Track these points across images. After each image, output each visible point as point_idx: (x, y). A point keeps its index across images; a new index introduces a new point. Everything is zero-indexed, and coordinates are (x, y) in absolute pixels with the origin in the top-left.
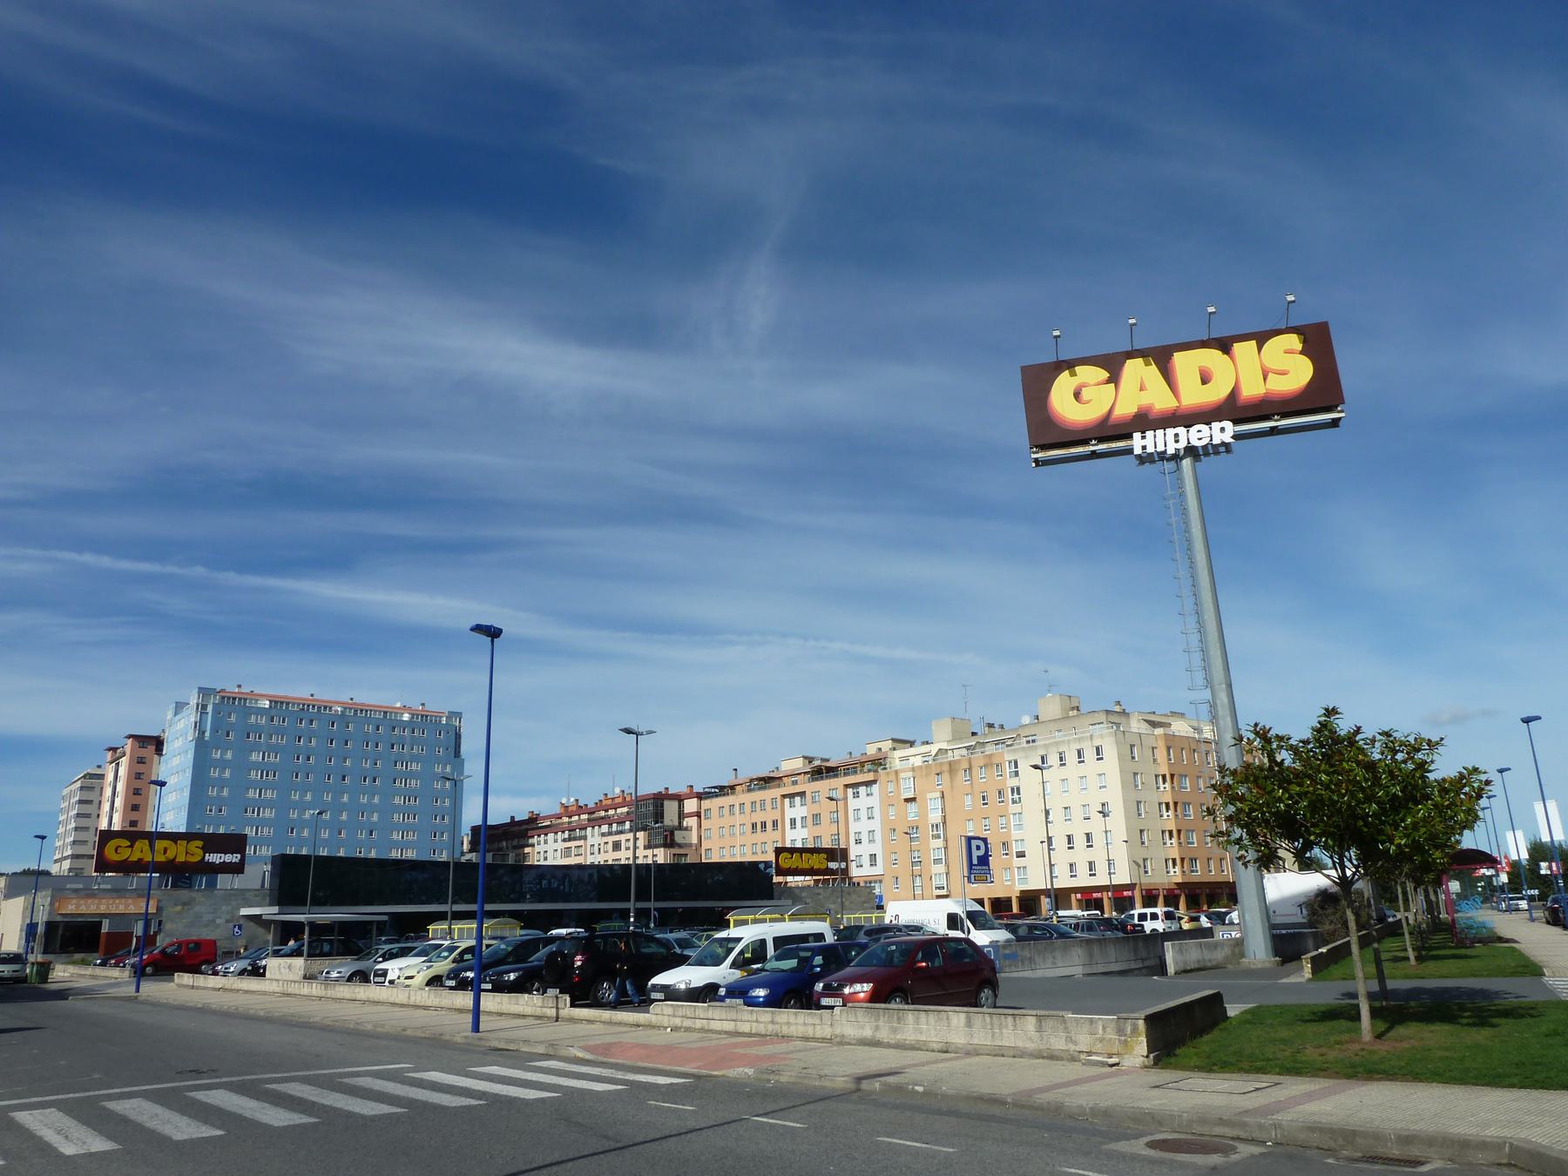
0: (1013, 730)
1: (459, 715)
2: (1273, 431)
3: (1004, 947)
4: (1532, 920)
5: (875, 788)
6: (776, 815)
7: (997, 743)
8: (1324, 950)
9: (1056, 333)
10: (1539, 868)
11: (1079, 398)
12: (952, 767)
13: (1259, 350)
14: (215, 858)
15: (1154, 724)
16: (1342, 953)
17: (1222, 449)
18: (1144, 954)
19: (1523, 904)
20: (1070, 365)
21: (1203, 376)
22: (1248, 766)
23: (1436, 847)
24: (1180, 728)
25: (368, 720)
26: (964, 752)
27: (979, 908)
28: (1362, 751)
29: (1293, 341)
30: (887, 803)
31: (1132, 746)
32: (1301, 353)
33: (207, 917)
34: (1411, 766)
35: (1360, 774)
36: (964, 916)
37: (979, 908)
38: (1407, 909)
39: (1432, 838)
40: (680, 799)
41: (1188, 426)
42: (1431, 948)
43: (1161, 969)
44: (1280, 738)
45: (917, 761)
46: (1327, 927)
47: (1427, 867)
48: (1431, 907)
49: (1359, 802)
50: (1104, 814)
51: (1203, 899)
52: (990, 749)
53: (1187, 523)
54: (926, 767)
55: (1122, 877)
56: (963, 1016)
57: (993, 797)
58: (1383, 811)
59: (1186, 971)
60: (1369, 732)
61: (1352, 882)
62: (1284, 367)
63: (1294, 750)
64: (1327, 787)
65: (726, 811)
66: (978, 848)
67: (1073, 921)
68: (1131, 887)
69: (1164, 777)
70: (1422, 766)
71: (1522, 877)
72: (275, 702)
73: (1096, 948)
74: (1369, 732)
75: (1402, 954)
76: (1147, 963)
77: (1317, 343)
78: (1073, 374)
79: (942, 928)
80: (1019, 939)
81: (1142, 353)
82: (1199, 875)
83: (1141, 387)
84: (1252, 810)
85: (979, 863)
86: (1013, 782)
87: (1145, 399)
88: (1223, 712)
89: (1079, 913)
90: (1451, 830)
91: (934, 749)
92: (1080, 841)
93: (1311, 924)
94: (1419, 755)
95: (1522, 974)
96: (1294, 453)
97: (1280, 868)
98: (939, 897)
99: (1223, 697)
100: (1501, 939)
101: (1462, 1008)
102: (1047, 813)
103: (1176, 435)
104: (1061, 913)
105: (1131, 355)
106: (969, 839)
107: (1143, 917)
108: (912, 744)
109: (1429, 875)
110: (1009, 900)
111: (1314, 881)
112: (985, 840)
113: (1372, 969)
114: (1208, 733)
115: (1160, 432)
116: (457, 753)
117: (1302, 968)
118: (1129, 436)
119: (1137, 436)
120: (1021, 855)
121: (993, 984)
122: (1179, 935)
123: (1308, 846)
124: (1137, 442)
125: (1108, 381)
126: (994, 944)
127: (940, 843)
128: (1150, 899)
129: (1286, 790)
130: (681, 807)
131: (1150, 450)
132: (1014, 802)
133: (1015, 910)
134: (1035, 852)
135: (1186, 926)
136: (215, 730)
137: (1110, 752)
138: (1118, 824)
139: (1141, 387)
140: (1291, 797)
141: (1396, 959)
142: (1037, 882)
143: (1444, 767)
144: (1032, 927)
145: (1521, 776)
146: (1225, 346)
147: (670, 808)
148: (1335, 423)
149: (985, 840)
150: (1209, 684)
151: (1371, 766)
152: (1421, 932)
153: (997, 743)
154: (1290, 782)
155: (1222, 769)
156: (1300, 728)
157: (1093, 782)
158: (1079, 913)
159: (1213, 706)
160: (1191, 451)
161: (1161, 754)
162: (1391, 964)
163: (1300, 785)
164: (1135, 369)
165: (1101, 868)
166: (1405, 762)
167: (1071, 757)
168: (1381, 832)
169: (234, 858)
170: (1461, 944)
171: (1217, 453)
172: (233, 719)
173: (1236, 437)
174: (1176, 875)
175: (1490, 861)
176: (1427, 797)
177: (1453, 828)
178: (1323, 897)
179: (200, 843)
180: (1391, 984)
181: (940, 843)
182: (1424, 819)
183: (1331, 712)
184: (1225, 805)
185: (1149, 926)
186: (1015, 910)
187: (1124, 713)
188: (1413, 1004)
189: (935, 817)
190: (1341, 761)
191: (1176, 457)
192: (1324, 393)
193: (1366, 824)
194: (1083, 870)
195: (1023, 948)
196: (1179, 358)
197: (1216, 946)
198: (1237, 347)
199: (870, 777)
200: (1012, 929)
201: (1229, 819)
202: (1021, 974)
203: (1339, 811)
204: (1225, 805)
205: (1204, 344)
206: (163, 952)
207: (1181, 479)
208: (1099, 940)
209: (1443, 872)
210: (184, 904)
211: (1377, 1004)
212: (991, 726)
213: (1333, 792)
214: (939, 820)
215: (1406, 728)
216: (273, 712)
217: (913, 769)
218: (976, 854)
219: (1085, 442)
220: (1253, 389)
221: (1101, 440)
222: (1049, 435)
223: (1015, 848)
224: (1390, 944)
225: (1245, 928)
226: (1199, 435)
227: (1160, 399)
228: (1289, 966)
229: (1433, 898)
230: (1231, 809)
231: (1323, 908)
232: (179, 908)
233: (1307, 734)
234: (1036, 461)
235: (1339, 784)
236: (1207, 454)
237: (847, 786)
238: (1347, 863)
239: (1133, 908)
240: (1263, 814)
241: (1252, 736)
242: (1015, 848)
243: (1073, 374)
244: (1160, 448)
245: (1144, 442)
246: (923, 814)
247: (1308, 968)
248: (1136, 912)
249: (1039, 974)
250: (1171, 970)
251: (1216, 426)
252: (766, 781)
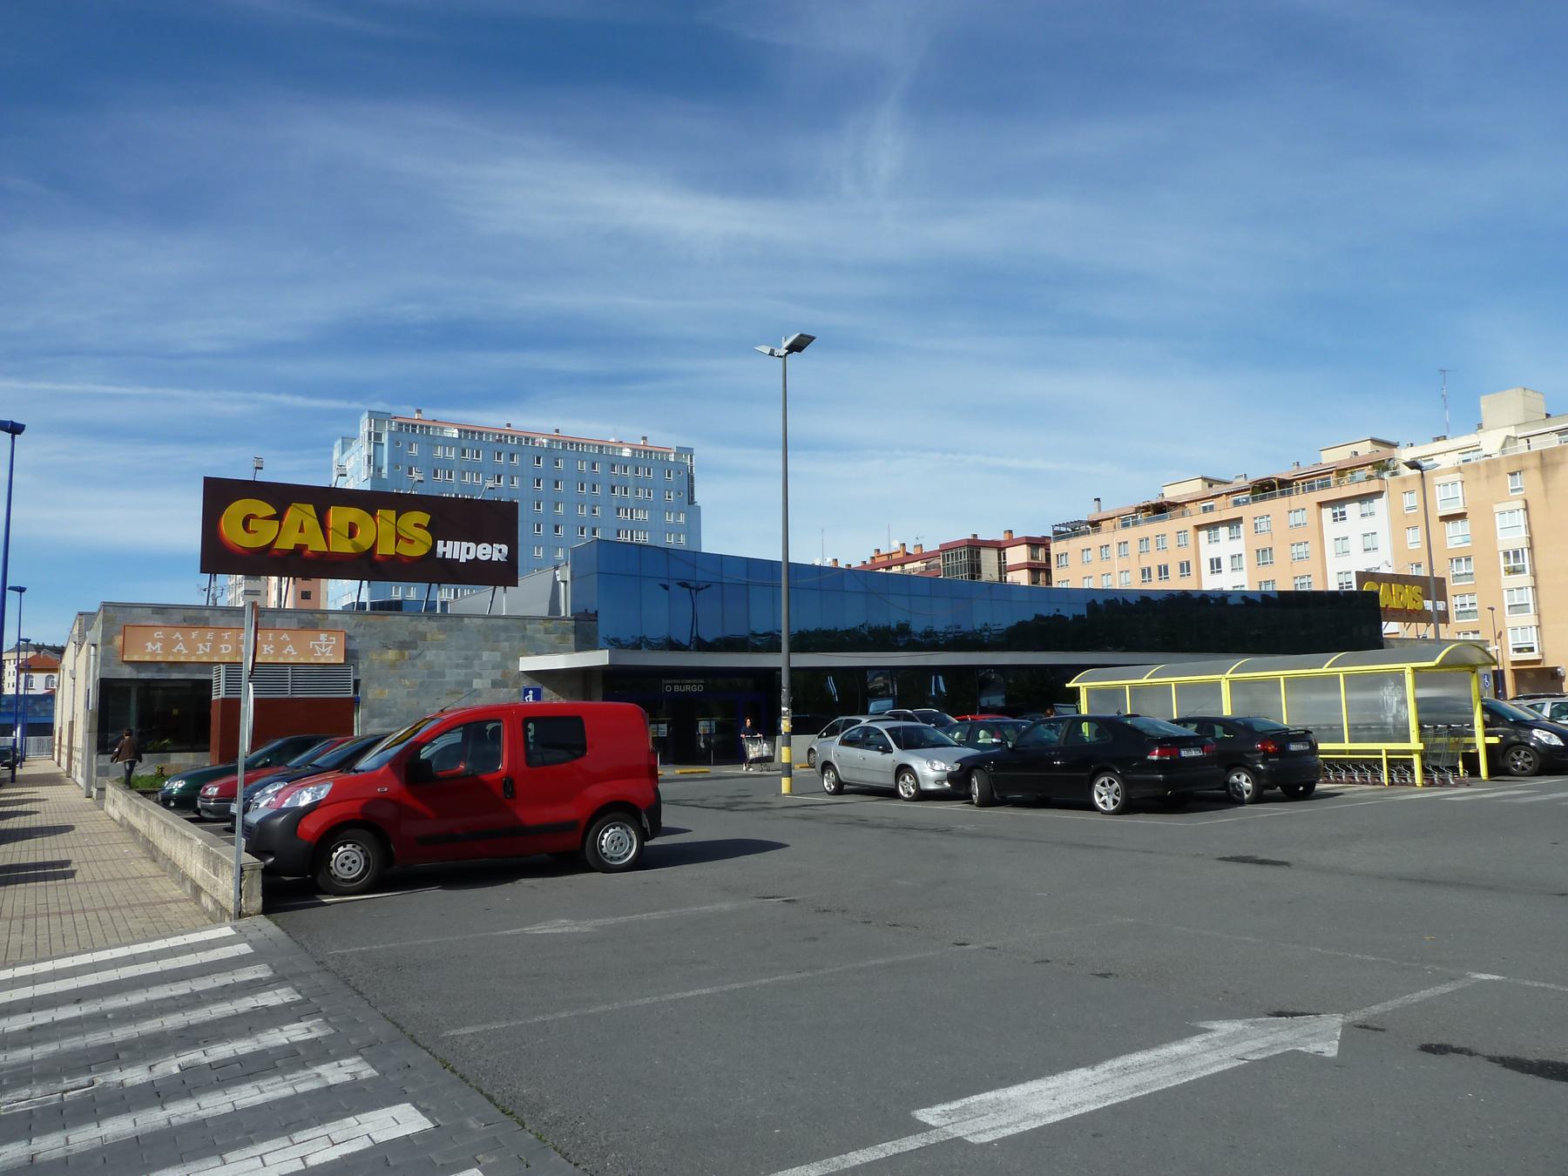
1: (690, 451)
5: (1379, 505)
6: (1186, 555)
14: (457, 550)
25: (581, 456)
30: (1400, 523)
33: (453, 676)
40: (1000, 547)
65: (1114, 549)
72: (465, 432)
116: (691, 501)
130: (1001, 557)
136: (394, 465)
147: (989, 559)
169: (493, 552)
172: (415, 451)
179: (424, 518)
199: (1374, 486)
206: (409, 765)
210: (402, 646)
214: (1524, 544)
216: (464, 443)
232: (392, 655)
237: (1321, 505)
252: (1160, 510)
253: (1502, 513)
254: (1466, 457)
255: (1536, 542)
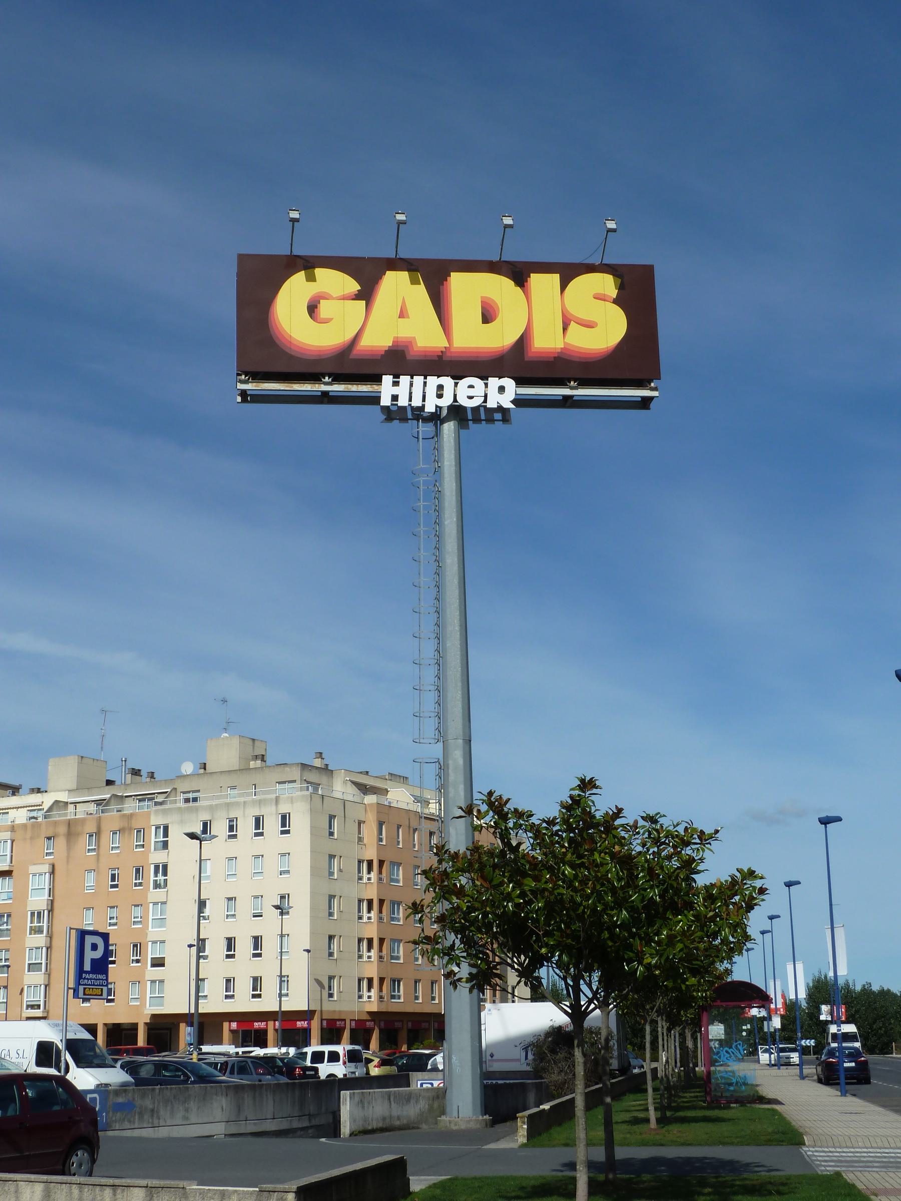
0: (167, 782)
2: (567, 402)
3: (117, 1093)
4: (802, 1077)
7: (142, 798)
8: (546, 1107)
9: (294, 215)
10: (819, 1012)
11: (314, 314)
12: (72, 830)
13: (563, 287)
15: (364, 789)
16: (564, 1113)
17: (498, 416)
18: (312, 1108)
19: (795, 1057)
20: (308, 264)
21: (488, 311)
22: (476, 849)
23: (695, 972)
24: (400, 797)
26: (92, 808)
27: (87, 1036)
28: (621, 841)
29: (607, 284)
31: (332, 817)
32: (615, 301)
34: (675, 863)
35: (613, 871)
36: (61, 1046)
37: (87, 1036)
38: (655, 1059)
39: (689, 957)
41: (457, 377)
42: (679, 1108)
43: (334, 1130)
44: (518, 814)
45: (20, 817)
46: (554, 1077)
47: (684, 1000)
48: (687, 1057)
49: (606, 906)
50: (282, 910)
51: (403, 1035)
52: (130, 806)
53: (439, 511)
54: (33, 823)
55: (297, 1002)
56: (39, 1188)
57: (127, 877)
58: (635, 920)
59: (366, 1132)
60: (630, 816)
61: (586, 1014)
62: (586, 317)
63: (536, 831)
64: (570, 885)
66: (94, 947)
67: (223, 1059)
68: (308, 1015)
69: (370, 863)
70: (690, 866)
71: (801, 1023)
73: (248, 1099)
74: (630, 816)
75: (641, 1115)
76: (315, 1122)
77: (637, 292)
78: (311, 278)
79: (27, 1064)
80: (140, 1082)
81: (409, 265)
82: (403, 1001)
83: (400, 313)
84: (471, 909)
85: (94, 967)
86: (159, 857)
87: (405, 330)
88: (456, 777)
89: (232, 1049)
90: (715, 954)
91: (47, 800)
92: (244, 947)
93: (537, 1073)
94: (688, 851)
95: (780, 1142)
96: (594, 432)
97: (506, 995)
98: (28, 1019)
99: (457, 757)
100: (762, 1099)
101: (703, 1183)
102: (202, 904)
103: (440, 387)
104: (205, 1048)
105: (394, 264)
106: (83, 934)
107: (318, 1057)
108: (15, 790)
109: (687, 1014)
110: (134, 1027)
111: (548, 1016)
112: (105, 936)
113: (600, 1133)
114: (433, 808)
115: (418, 380)
117: (515, 1131)
118: (376, 379)
119: (387, 379)
120: (158, 963)
121: (91, 1144)
122: (367, 1082)
123: (537, 961)
124: (386, 389)
125: (358, 297)
126: (102, 1089)
127: (40, 940)
128: (331, 1034)
129: (518, 884)
131: (403, 402)
132: (157, 886)
133: (141, 1042)
134: (179, 958)
135: (375, 1071)
137: (301, 823)
138: (300, 926)
139: (400, 313)
140: (523, 895)
141: (636, 1121)
142: (176, 1003)
143: (714, 869)
144: (161, 1066)
145: (811, 897)
146: (519, 274)
148: (645, 403)
149: (105, 936)
150: (441, 735)
151: (627, 861)
152: (668, 1088)
153: (142, 798)
154: (524, 875)
155: (441, 851)
156: (545, 806)
157: (272, 864)
158: (232, 1049)
159: (443, 768)
160: (457, 411)
161: (369, 832)
162: (624, 1127)
163: (537, 879)
164: (396, 285)
165: (270, 987)
166: (669, 858)
167: (246, 827)
168: (630, 947)
170: (716, 1103)
171: (490, 420)
173: (519, 402)
174: (371, 1002)
175: (761, 997)
176: (690, 906)
177: (718, 949)
178: (556, 1039)
180: (621, 1153)
181: (40, 940)
182: (683, 933)
183: (587, 784)
184: (438, 899)
185: (325, 1070)
186: (141, 1042)
187: (326, 770)
188: (646, 1177)
189: (38, 900)
190: (592, 851)
191: (436, 418)
192: (635, 361)
193: (613, 936)
194: (243, 988)
195: (143, 1096)
196: (458, 281)
197: (409, 1098)
198: (535, 279)
200: (131, 1068)
201: (441, 919)
202: (136, 1133)
203: (581, 918)
204: (438, 899)
205: (492, 267)
207: (438, 449)
208: (253, 1087)
209: (703, 1009)
211: (601, 1177)
212: (136, 773)
213: (575, 890)
215: (674, 817)
217: (13, 829)
218: (89, 955)
219: (316, 378)
220: (547, 340)
221: (338, 378)
222: (266, 359)
223: (151, 953)
224: (631, 1102)
225: (451, 1077)
226: (470, 392)
227: (426, 335)
228: (500, 1128)
229: (690, 1044)
230: (443, 907)
231: (553, 1051)
233: (553, 811)
234: (244, 394)
235: (584, 882)
236: (477, 420)
238: (584, 987)
239: (307, 1043)
240: (485, 915)
241: (484, 808)
242: (151, 953)
243: (311, 278)
244: (417, 402)
245: (395, 391)
246: (21, 896)
247: (523, 1129)
248: (309, 1050)
249: (163, 1132)
250: (346, 1129)
251: (494, 383)
253: (34, 875)
254: (34, 814)
255: (56, 905)
